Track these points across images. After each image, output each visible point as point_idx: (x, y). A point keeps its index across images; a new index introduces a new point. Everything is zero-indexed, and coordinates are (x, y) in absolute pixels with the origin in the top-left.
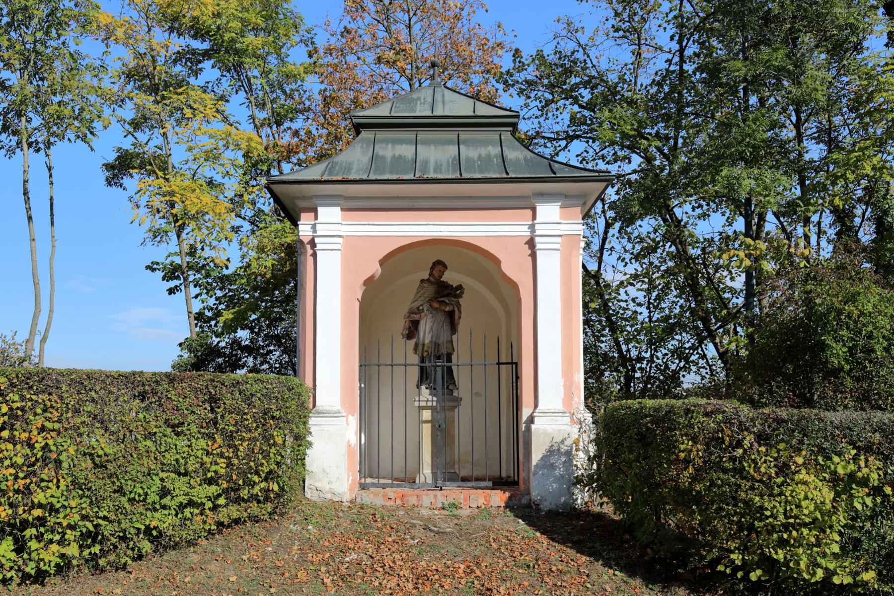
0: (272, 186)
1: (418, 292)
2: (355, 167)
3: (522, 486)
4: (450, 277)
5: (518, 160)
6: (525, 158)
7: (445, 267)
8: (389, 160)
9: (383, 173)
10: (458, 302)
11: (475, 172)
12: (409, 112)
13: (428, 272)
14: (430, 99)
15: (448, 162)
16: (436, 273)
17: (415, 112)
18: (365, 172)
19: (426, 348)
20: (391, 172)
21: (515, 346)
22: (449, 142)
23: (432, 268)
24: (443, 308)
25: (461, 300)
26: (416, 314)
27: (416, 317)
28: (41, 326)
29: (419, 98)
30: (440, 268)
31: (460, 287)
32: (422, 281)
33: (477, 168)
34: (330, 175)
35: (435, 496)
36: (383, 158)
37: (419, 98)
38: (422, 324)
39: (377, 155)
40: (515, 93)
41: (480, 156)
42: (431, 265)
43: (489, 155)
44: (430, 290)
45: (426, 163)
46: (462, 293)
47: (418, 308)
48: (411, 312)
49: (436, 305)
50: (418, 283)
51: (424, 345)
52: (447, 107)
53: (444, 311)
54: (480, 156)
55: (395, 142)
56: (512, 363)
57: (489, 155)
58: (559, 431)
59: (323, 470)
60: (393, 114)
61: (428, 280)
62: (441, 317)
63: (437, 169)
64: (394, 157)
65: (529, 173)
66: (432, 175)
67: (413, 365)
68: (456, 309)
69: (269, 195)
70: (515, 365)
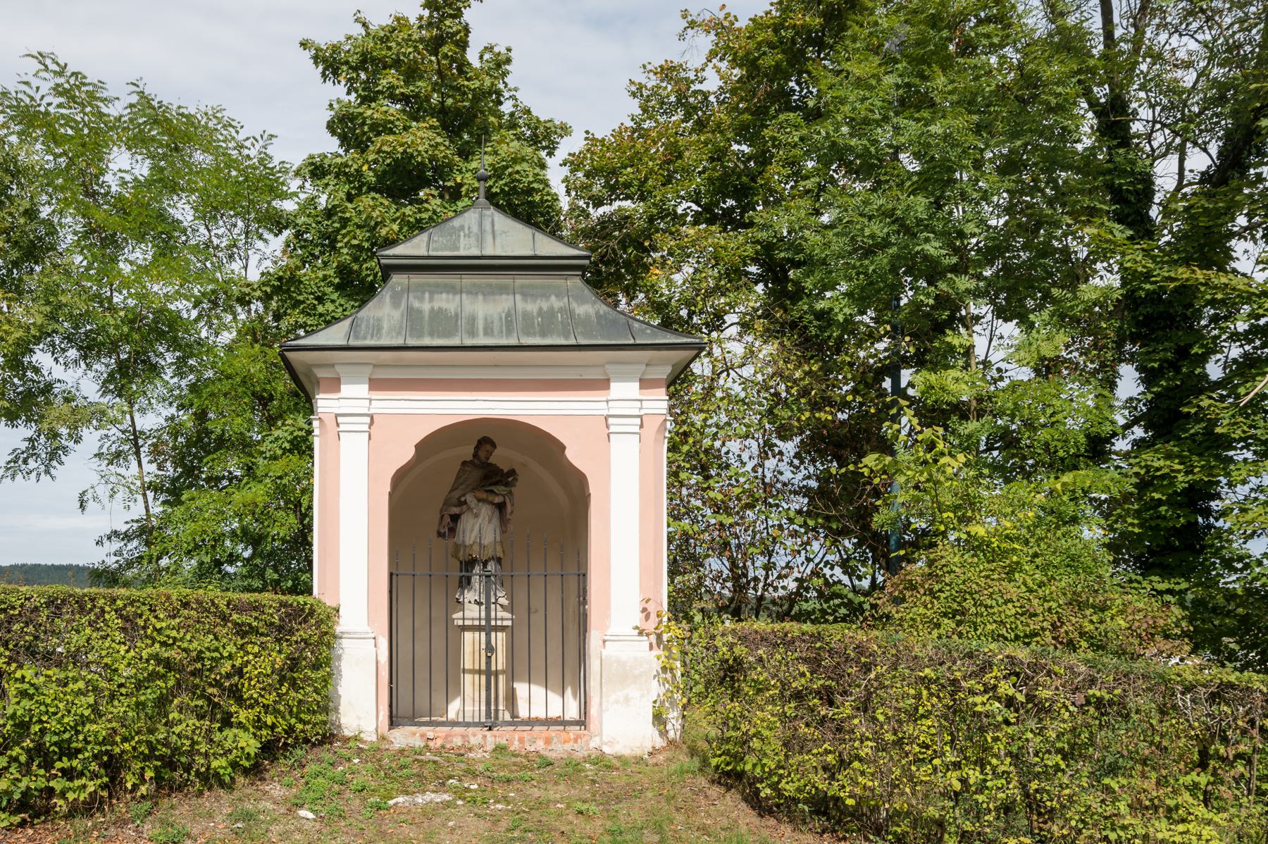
0: (288, 354)
1: (458, 477)
2: (385, 326)
4: (501, 457)
5: (588, 316)
6: (597, 313)
7: (494, 445)
8: (426, 315)
9: (420, 336)
10: (510, 492)
11: (534, 335)
12: (451, 250)
13: (472, 451)
14: (475, 229)
15: (501, 319)
17: (458, 249)
18: (399, 333)
20: (431, 334)
23: (477, 448)
24: (490, 498)
25: (513, 489)
28: (394, 686)
29: (462, 228)
30: (488, 447)
31: (512, 472)
32: (464, 463)
33: (537, 329)
34: (357, 338)
35: (485, 737)
36: (420, 311)
37: (462, 228)
41: (540, 309)
43: (551, 309)
44: (477, 474)
46: (516, 480)
48: (447, 503)
52: (498, 240)
54: (540, 309)
55: (435, 290)
57: (551, 309)
60: (432, 253)
61: (471, 462)
63: (488, 331)
64: (432, 310)
65: (603, 338)
69: (287, 376)
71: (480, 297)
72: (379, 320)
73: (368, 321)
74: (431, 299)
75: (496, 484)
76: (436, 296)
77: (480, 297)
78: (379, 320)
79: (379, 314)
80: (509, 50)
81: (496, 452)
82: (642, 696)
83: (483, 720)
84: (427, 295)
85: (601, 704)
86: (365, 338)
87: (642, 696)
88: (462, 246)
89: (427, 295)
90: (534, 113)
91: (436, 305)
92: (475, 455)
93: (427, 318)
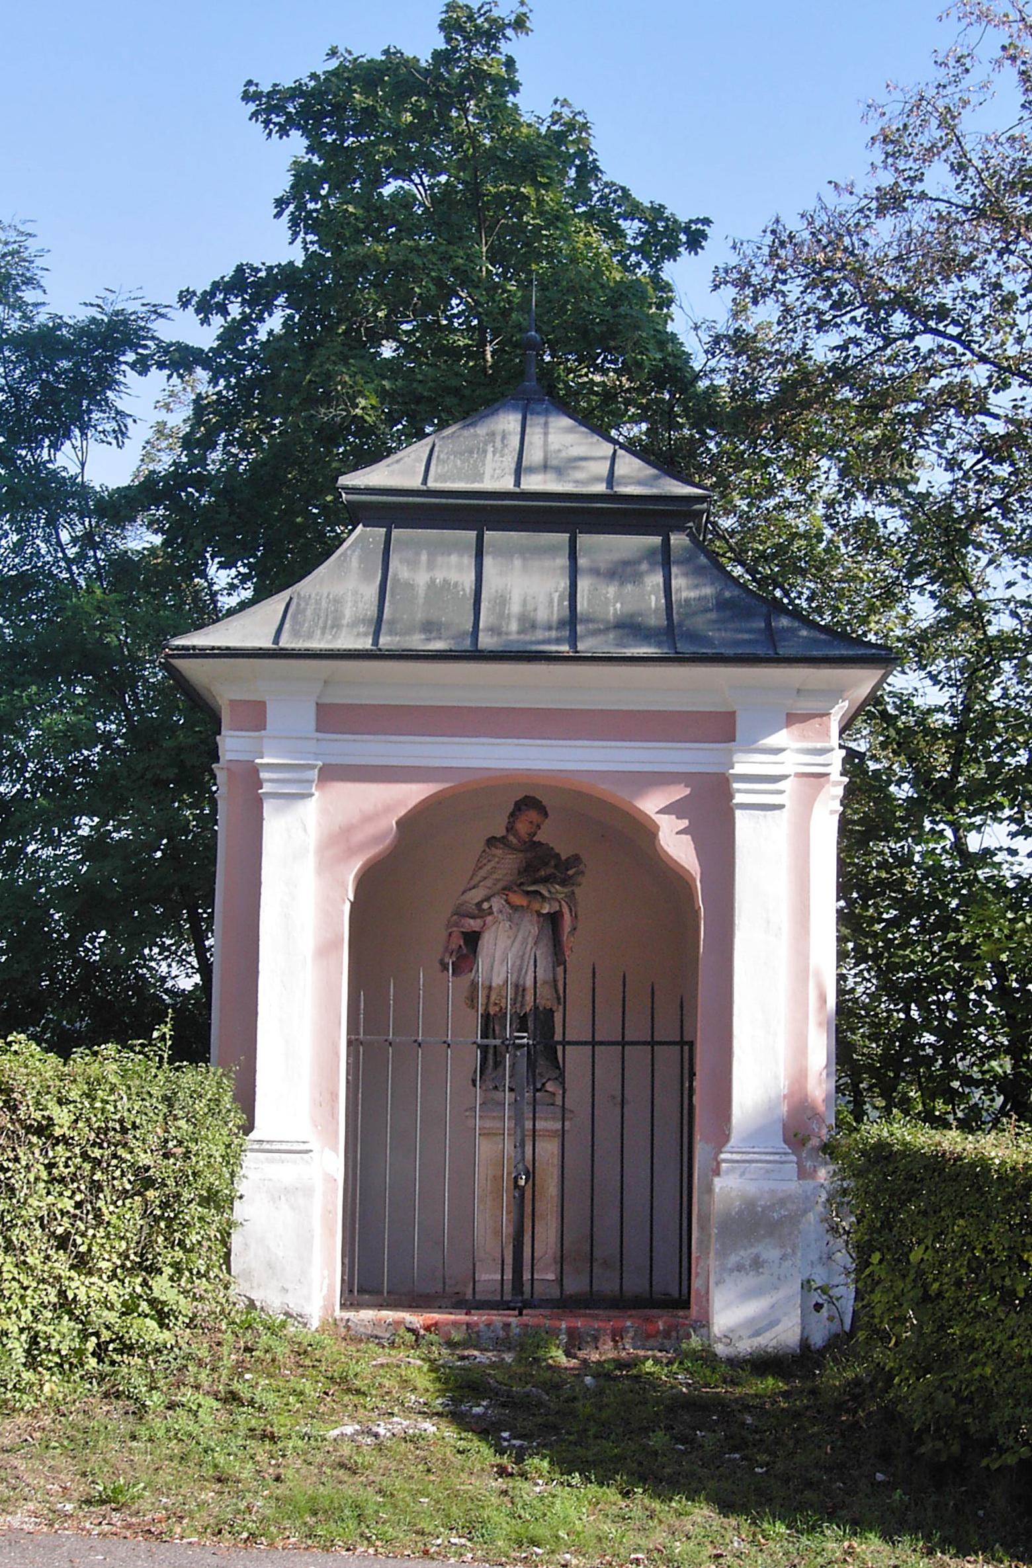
0: (177, 663)
2: (348, 614)
3: (694, 1310)
7: (543, 811)
8: (421, 592)
12: (468, 479)
15: (551, 602)
16: (522, 827)
17: (480, 477)
19: (493, 997)
21: (684, 1008)
22: (551, 550)
24: (536, 906)
25: (577, 890)
26: (473, 917)
27: (473, 924)
30: (533, 815)
31: (576, 859)
32: (491, 842)
38: (486, 943)
39: (396, 580)
40: (753, 308)
42: (511, 808)
44: (507, 864)
45: (502, 601)
47: (479, 904)
48: (461, 913)
49: (518, 900)
50: (481, 846)
51: (490, 988)
53: (539, 914)
56: (682, 1043)
58: (773, 1191)
59: (270, 1266)
62: (530, 927)
66: (528, 430)
67: (562, 1290)
68: (566, 910)
70: (687, 1045)
71: (517, 562)
72: (337, 601)
73: (318, 602)
74: (431, 566)
75: (545, 880)
76: (440, 559)
77: (517, 562)
78: (337, 601)
79: (338, 589)
80: (241, 1197)
81: (547, 825)
82: (784, 1258)
83: (508, 1297)
84: (424, 557)
85: (681, 1267)
86: (310, 636)
87: (784, 1258)
88: (488, 471)
89: (424, 557)
90: (634, 194)
91: (439, 578)
92: (510, 829)
93: (421, 601)
